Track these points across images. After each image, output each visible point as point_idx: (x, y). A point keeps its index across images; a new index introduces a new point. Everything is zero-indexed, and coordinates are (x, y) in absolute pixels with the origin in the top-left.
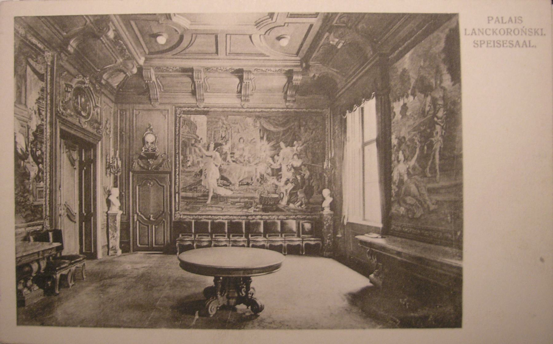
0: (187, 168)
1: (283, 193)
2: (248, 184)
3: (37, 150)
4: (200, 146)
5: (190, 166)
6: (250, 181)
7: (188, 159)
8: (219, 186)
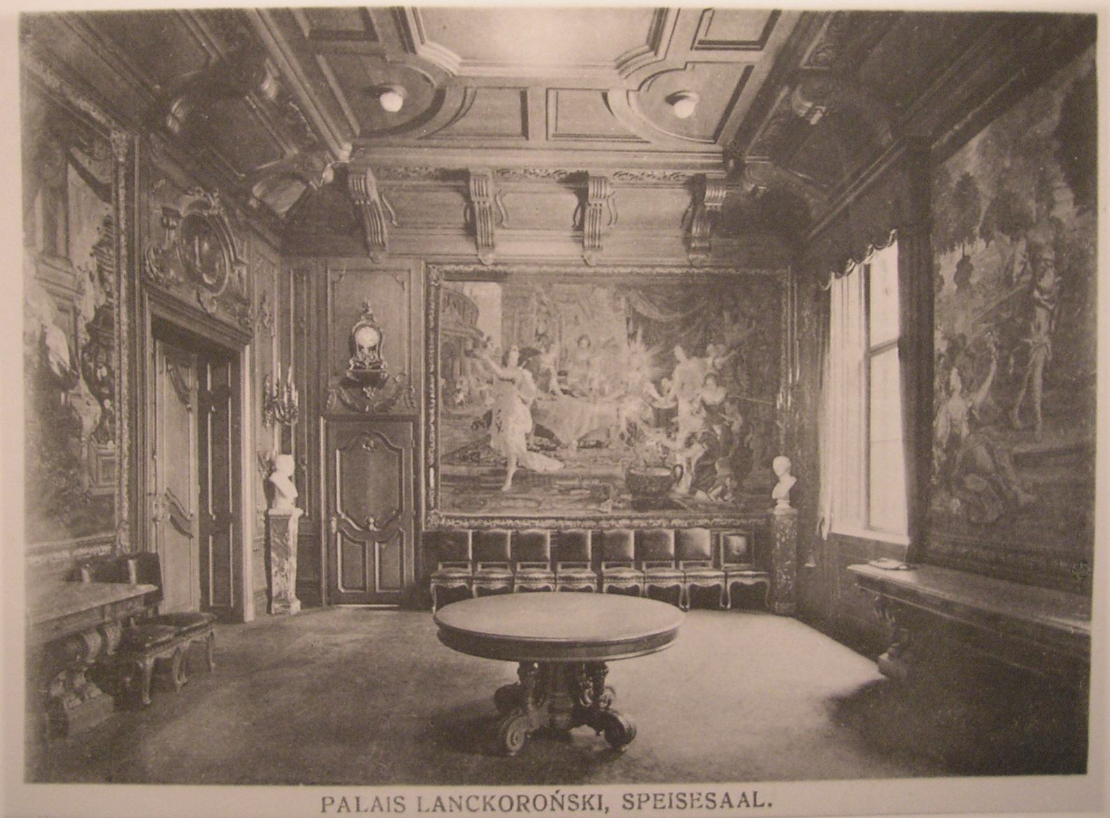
0: (454, 406)
1: (682, 467)
2: (599, 445)
3: (97, 366)
4: (486, 356)
5: (461, 403)
6: (603, 438)
7: (458, 386)
8: (529, 450)
